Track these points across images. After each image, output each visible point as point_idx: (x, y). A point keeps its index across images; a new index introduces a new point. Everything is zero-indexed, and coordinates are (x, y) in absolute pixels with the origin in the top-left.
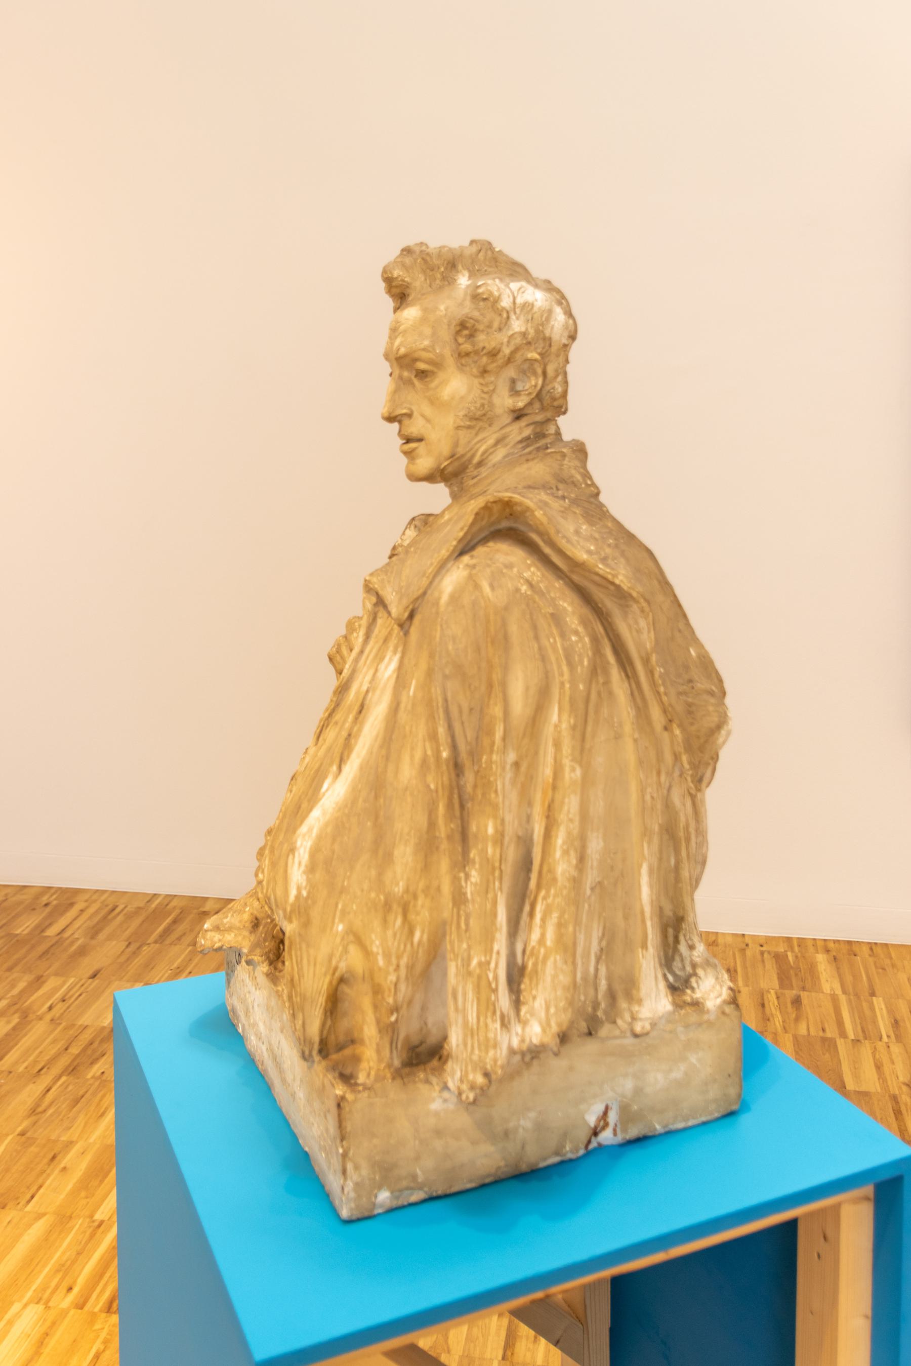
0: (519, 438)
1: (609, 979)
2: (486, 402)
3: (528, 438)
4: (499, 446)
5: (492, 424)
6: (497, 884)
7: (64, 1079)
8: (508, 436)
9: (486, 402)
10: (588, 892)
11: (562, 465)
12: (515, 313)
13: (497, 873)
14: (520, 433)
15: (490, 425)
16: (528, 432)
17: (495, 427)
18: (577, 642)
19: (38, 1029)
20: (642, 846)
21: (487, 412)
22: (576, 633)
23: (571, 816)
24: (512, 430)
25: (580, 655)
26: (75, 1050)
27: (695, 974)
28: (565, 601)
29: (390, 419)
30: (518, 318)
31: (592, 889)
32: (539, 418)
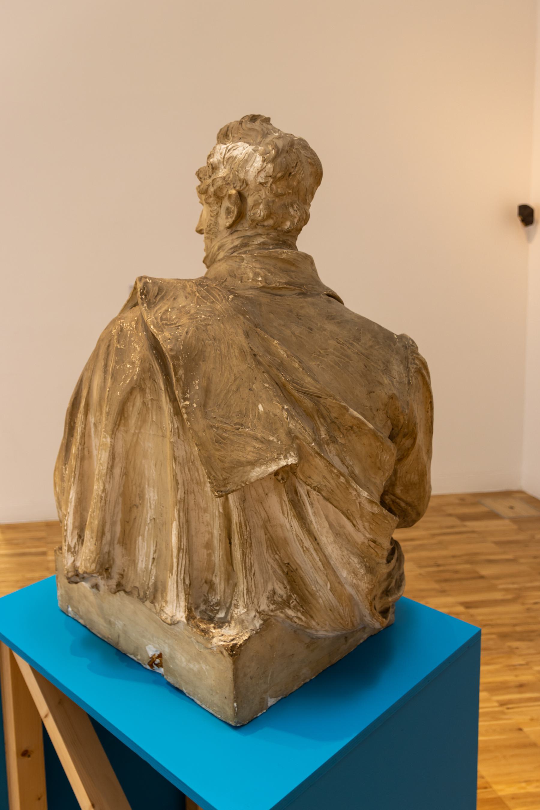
0: (232, 246)
1: (156, 577)
2: (213, 222)
3: (236, 246)
4: (220, 251)
5: (217, 236)
6: (72, 479)
7: (494, 636)
8: (225, 245)
9: (213, 222)
10: (149, 521)
11: (241, 266)
12: (224, 164)
13: (73, 474)
14: (232, 243)
15: (216, 237)
16: (237, 242)
17: (218, 239)
18: (129, 368)
19: (516, 608)
20: (174, 511)
21: (211, 229)
22: (133, 363)
23: (101, 462)
24: (227, 241)
25: (127, 377)
26: (518, 629)
27: (229, 622)
28: (138, 344)
29: (200, 232)
30: (225, 168)
31: (151, 520)
32: (249, 233)
